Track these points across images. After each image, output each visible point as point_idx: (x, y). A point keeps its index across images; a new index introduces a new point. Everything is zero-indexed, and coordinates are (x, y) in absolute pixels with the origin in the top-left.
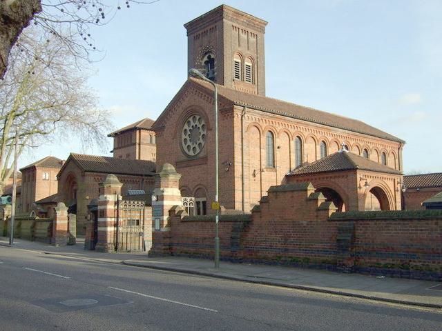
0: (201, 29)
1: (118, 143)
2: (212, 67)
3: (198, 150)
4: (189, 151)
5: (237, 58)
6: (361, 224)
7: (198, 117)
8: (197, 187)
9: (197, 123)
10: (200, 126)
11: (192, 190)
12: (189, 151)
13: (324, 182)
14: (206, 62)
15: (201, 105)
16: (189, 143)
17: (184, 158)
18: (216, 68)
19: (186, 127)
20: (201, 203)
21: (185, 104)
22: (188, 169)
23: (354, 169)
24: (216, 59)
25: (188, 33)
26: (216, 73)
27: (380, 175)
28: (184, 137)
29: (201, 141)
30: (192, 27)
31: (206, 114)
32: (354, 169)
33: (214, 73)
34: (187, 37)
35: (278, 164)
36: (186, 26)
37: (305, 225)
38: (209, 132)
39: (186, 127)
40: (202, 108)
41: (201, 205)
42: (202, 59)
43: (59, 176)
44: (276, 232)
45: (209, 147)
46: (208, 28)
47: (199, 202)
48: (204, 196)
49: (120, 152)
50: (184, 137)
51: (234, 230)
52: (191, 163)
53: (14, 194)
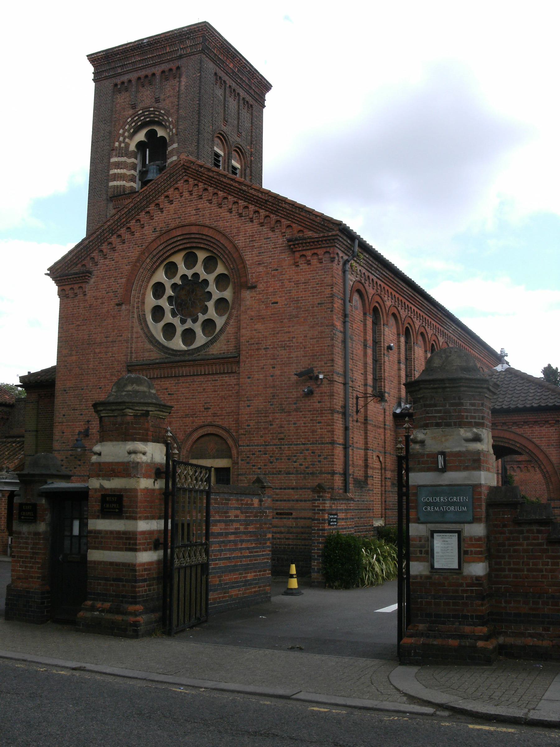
0: (136, 70)
3: (201, 339)
9: (199, 268)
10: (211, 278)
14: (141, 146)
15: (221, 224)
16: (168, 318)
17: (155, 355)
23: (334, 346)
28: (151, 301)
29: (212, 313)
31: (235, 247)
32: (334, 346)
34: (93, 84)
39: (160, 276)
42: (132, 136)
46: (157, 70)
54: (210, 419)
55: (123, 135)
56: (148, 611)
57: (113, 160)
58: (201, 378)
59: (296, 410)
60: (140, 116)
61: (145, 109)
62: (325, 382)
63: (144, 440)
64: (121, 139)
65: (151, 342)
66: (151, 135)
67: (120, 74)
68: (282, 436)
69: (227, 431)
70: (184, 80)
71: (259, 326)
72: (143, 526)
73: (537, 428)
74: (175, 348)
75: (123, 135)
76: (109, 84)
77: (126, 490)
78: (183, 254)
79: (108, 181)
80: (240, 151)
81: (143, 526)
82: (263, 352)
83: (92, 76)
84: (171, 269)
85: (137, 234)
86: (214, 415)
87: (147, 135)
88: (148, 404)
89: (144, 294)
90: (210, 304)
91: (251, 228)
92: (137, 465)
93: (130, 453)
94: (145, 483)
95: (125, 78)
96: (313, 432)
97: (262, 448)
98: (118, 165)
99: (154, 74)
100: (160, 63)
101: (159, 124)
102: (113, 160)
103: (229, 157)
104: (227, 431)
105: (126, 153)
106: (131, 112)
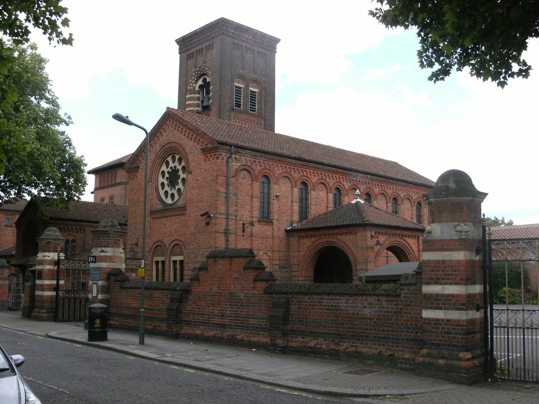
1: (100, 183)
2: (208, 93)
3: (177, 197)
4: (166, 197)
5: (239, 83)
6: (296, 298)
7: (177, 157)
8: (155, 246)
9: (177, 164)
11: (167, 246)
12: (166, 197)
13: (330, 239)
14: (200, 86)
16: (167, 188)
17: (160, 206)
18: (211, 94)
19: (164, 168)
20: (178, 262)
21: (163, 139)
22: (164, 220)
24: (211, 83)
25: (180, 49)
26: (211, 101)
27: (398, 232)
28: (161, 180)
30: (186, 44)
33: (209, 100)
34: (179, 55)
35: (275, 216)
36: (178, 41)
37: (242, 297)
38: (189, 176)
39: (164, 168)
40: (181, 146)
41: (178, 265)
42: (196, 82)
43: (18, 224)
44: (213, 304)
45: (188, 194)
47: (176, 261)
48: (181, 254)
49: (106, 194)
50: (161, 180)
51: (172, 300)
52: (168, 214)
53: (458, 199)
54: (177, 237)
55: (191, 82)
56: (48, 312)
57: (188, 96)
58: (174, 218)
59: (204, 232)
60: (198, 71)
61: (200, 68)
62: (214, 218)
63: (49, 251)
64: (191, 84)
65: (159, 200)
66: (205, 80)
67: (189, 49)
68: (199, 245)
69: (182, 242)
70: (215, 50)
71: (193, 192)
72: (47, 282)
73: (348, 236)
74: (168, 203)
75: (191, 82)
76: (185, 55)
77: (42, 269)
78: (170, 157)
79: (185, 108)
80: (256, 82)
81: (47, 282)
82: (194, 204)
83: (178, 51)
84: (167, 163)
85: (154, 148)
86: (178, 235)
87: (203, 81)
88: (49, 239)
89: (158, 177)
90: (180, 181)
91: (191, 143)
92: (46, 261)
93: (44, 256)
94: (48, 267)
95: (191, 51)
96: (210, 242)
97: (192, 251)
98: (190, 99)
99: (203, 48)
100: (205, 42)
101: (206, 74)
102: (188, 96)
103: (247, 87)
104: (182, 242)
105: (194, 92)
106: (194, 69)
